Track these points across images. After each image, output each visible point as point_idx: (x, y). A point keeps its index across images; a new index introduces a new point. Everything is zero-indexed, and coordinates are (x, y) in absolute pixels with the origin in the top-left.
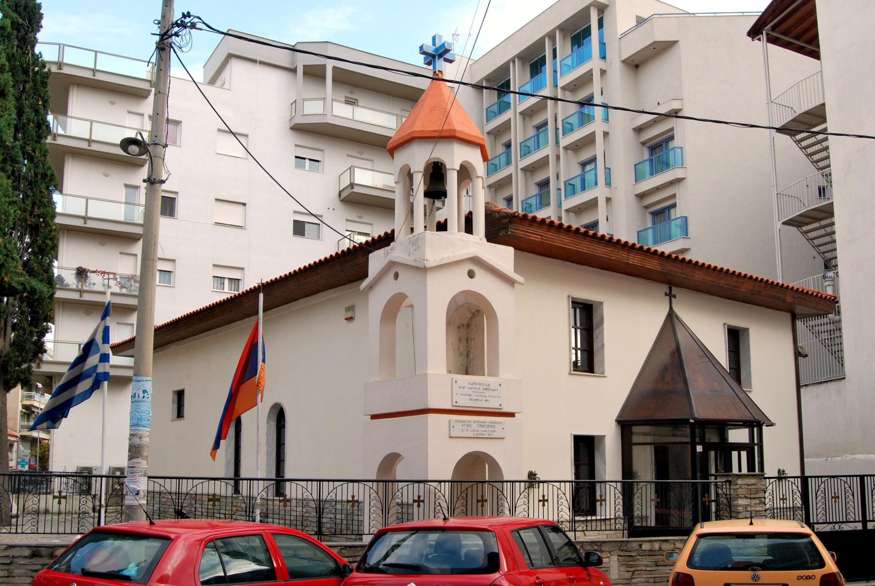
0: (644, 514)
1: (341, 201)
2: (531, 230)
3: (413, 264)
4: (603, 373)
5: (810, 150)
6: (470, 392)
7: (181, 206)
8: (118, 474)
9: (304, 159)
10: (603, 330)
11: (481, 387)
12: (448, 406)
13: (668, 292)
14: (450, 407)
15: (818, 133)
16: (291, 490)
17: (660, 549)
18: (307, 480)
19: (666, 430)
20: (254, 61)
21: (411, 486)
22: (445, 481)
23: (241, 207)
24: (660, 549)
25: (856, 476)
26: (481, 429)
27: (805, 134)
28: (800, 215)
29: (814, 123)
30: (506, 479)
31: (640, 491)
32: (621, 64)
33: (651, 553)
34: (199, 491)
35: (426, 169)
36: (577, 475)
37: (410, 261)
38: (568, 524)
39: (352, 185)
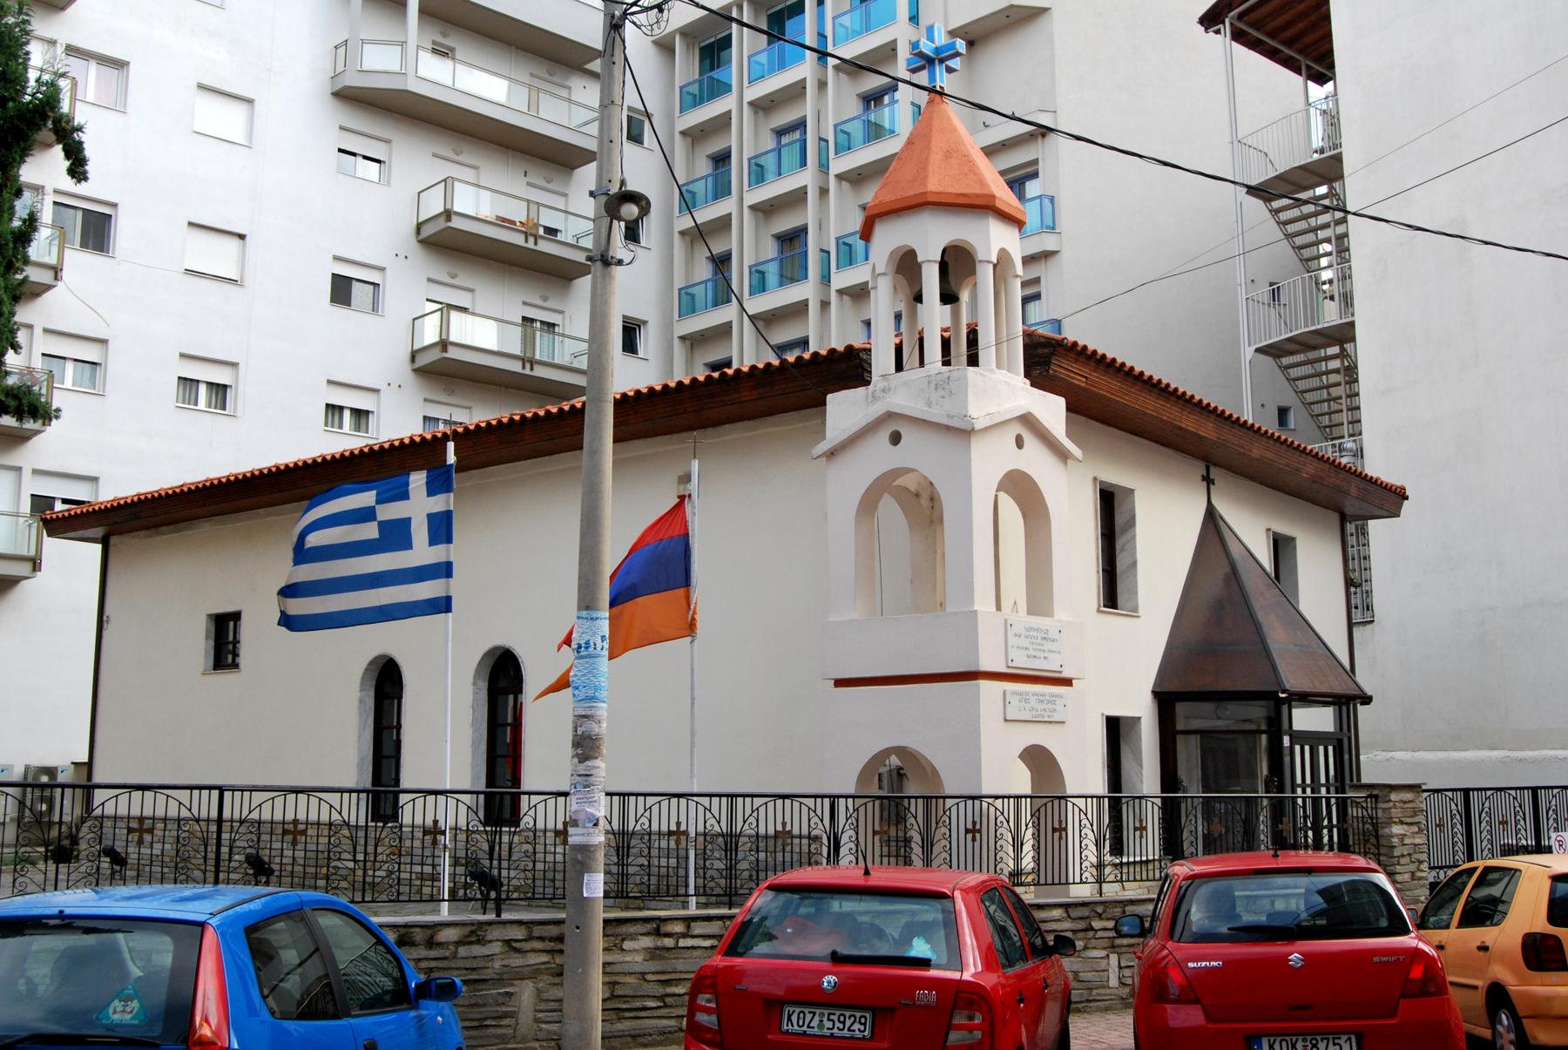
1: (420, 242)
2: (1075, 367)
3: (945, 421)
4: (1135, 609)
5: (1291, 228)
7: (123, 232)
8: (45, 779)
9: (354, 154)
10: (1134, 537)
12: (1001, 668)
15: (1306, 202)
16: (413, 813)
19: (1208, 707)
21: (551, 802)
23: (235, 242)
27: (1285, 202)
28: (1288, 340)
29: (1306, 183)
30: (948, 792)
34: (266, 816)
36: (491, 781)
37: (937, 414)
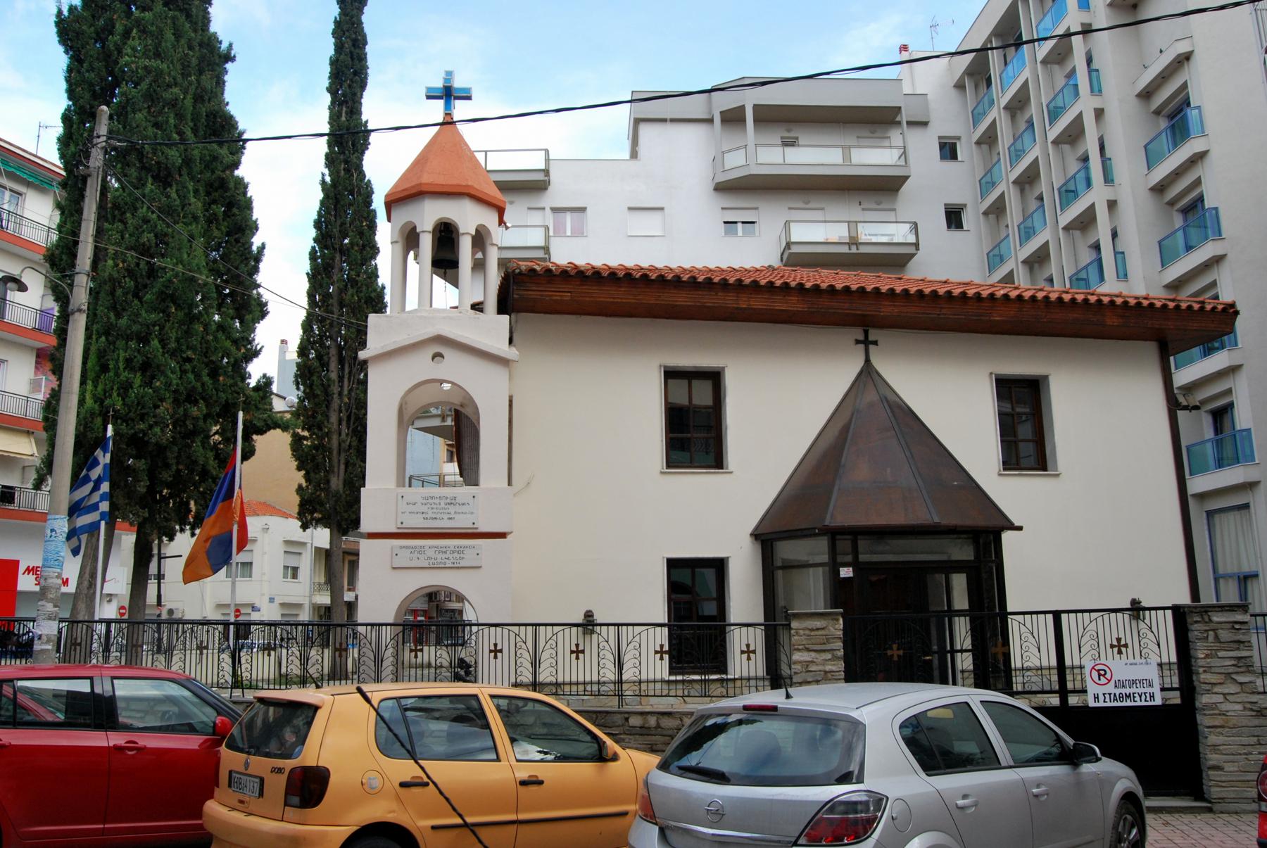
0: (254, 676)
6: (424, 509)
11: (442, 502)
13: (861, 338)
14: (394, 530)
17: (658, 726)
18: (519, 625)
20: (664, 120)
22: (386, 625)
24: (658, 726)
25: (1045, 613)
26: (440, 556)
31: (637, 639)
32: (1108, 10)
33: (644, 731)
35: (434, 230)
38: (612, 686)
39: (789, 245)
